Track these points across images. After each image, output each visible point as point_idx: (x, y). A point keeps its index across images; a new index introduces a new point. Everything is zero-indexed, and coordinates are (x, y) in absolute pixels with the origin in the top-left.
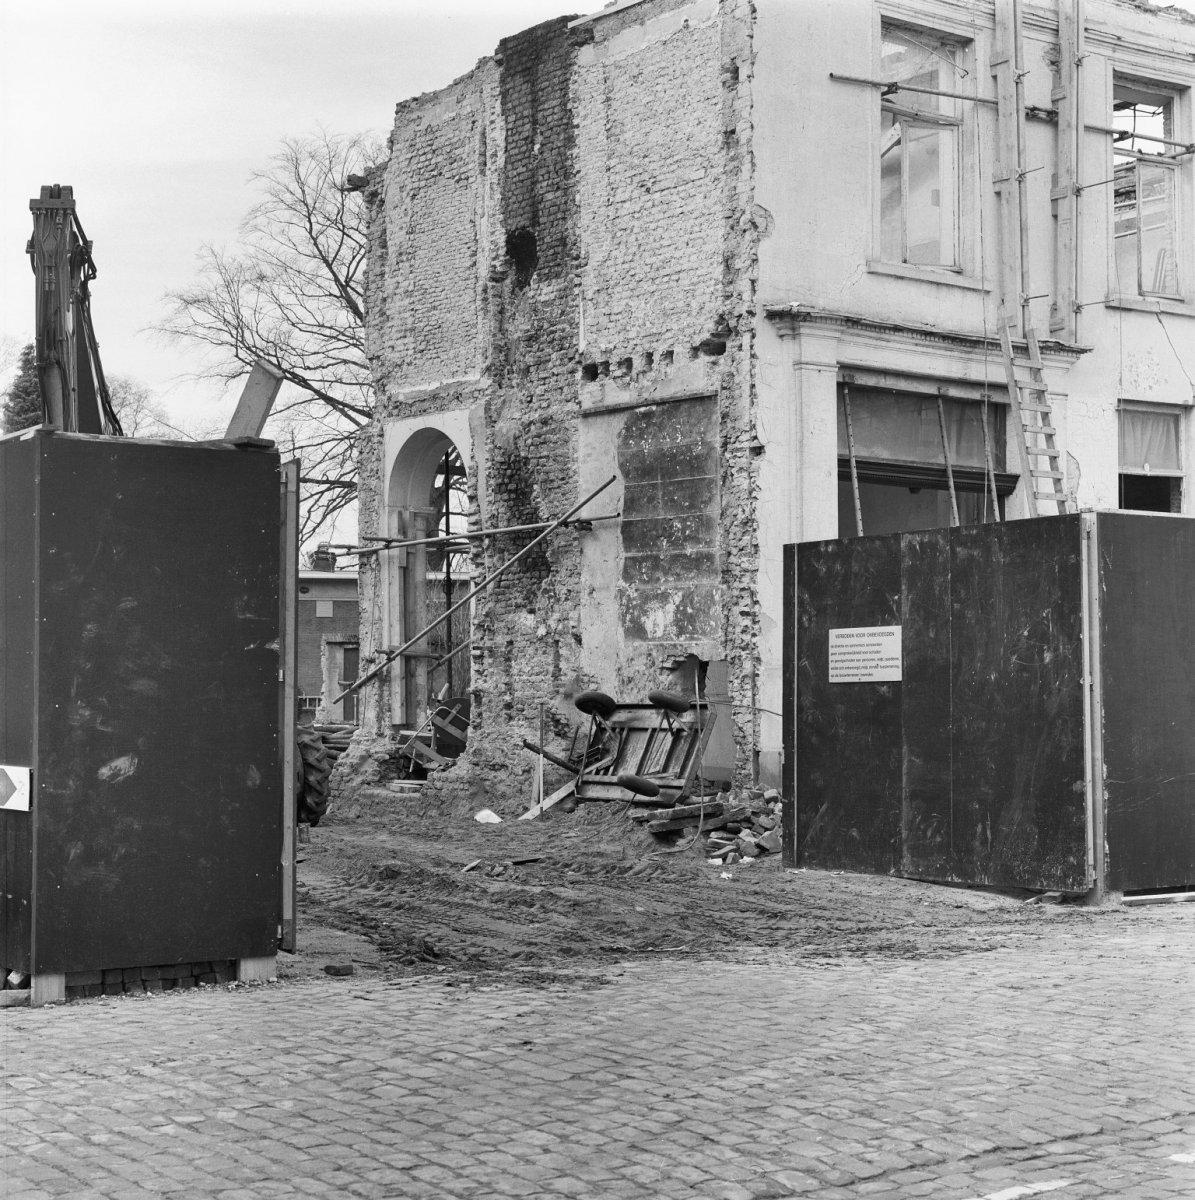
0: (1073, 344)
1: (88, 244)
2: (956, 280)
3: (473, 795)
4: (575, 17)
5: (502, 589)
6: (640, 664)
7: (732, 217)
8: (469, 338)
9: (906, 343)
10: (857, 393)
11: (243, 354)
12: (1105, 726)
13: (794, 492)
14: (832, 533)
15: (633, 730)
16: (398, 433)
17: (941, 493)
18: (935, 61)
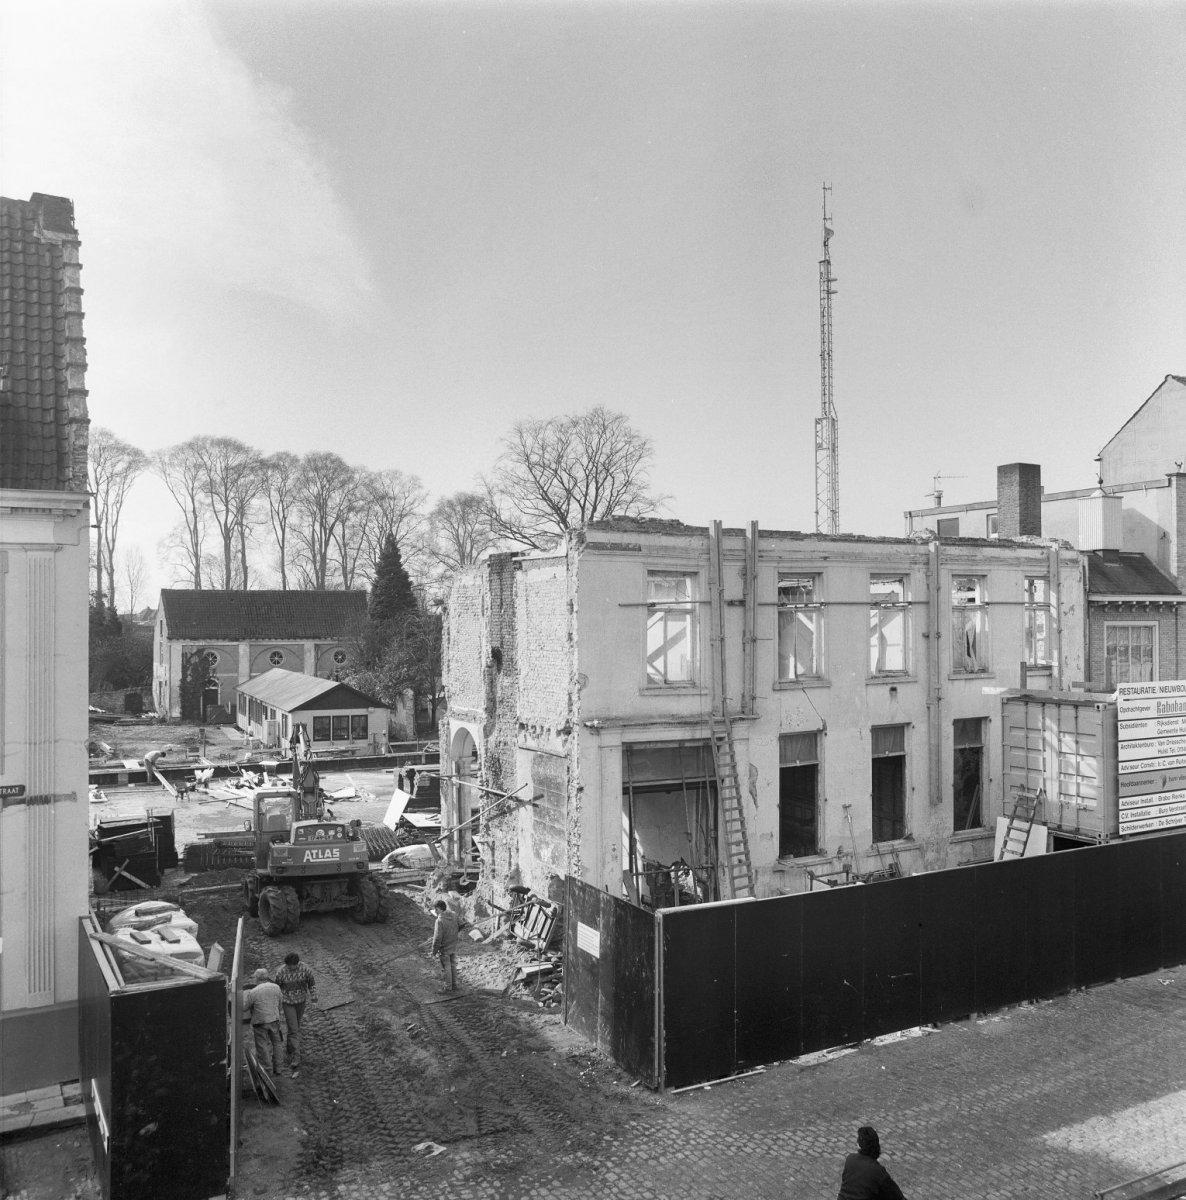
12: (665, 1013)
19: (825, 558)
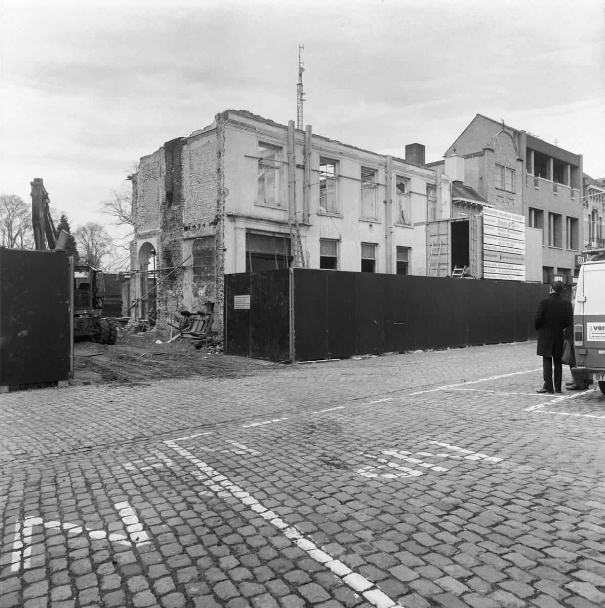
1: (47, 194)
2: (279, 207)
3: (157, 337)
4: (183, 138)
5: (165, 284)
6: (197, 304)
7: (219, 191)
8: (157, 219)
10: (251, 235)
11: (122, 218)
13: (234, 261)
14: (243, 270)
15: (194, 320)
16: (140, 243)
18: (273, 152)
19: (341, 153)
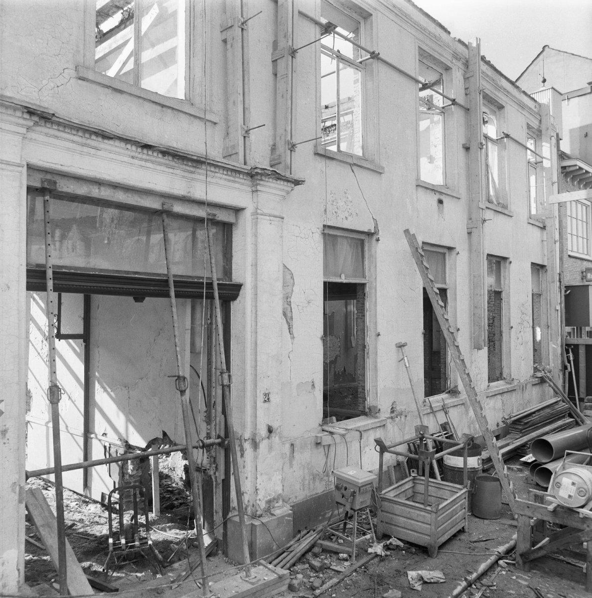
0: (288, 175)
9: (119, 154)
17: (199, 300)
